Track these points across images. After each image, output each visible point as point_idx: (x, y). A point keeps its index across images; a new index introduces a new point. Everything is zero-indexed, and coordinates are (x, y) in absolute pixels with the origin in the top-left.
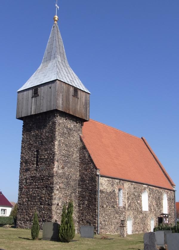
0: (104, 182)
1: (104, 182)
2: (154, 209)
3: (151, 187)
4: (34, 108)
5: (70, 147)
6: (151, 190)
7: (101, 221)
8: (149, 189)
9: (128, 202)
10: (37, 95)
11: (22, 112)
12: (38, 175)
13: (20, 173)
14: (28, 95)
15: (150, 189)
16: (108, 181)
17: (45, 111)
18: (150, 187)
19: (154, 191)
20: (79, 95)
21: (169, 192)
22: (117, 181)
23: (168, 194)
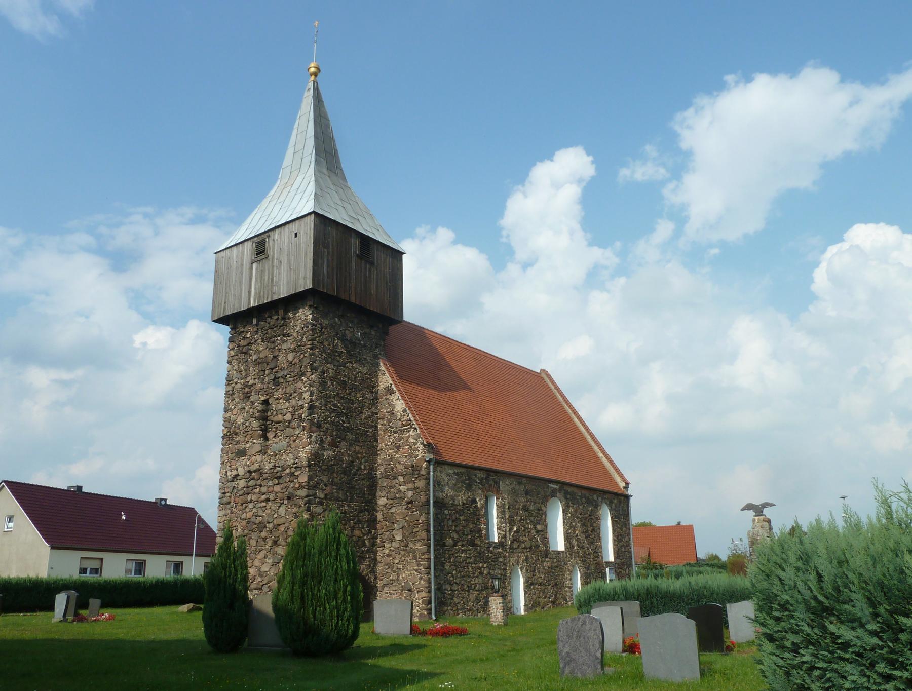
0: (446, 479)
1: (446, 479)
2: (578, 546)
3: (570, 490)
4: (256, 289)
5: (356, 389)
6: (569, 497)
7: (442, 582)
8: (565, 494)
9: (511, 530)
10: (263, 257)
11: (225, 303)
12: (268, 466)
13: (223, 463)
14: (242, 261)
15: (566, 493)
16: (457, 474)
17: (283, 295)
18: (566, 488)
19: (578, 498)
20: (376, 255)
21: (615, 501)
22: (480, 474)
23: (613, 505)
